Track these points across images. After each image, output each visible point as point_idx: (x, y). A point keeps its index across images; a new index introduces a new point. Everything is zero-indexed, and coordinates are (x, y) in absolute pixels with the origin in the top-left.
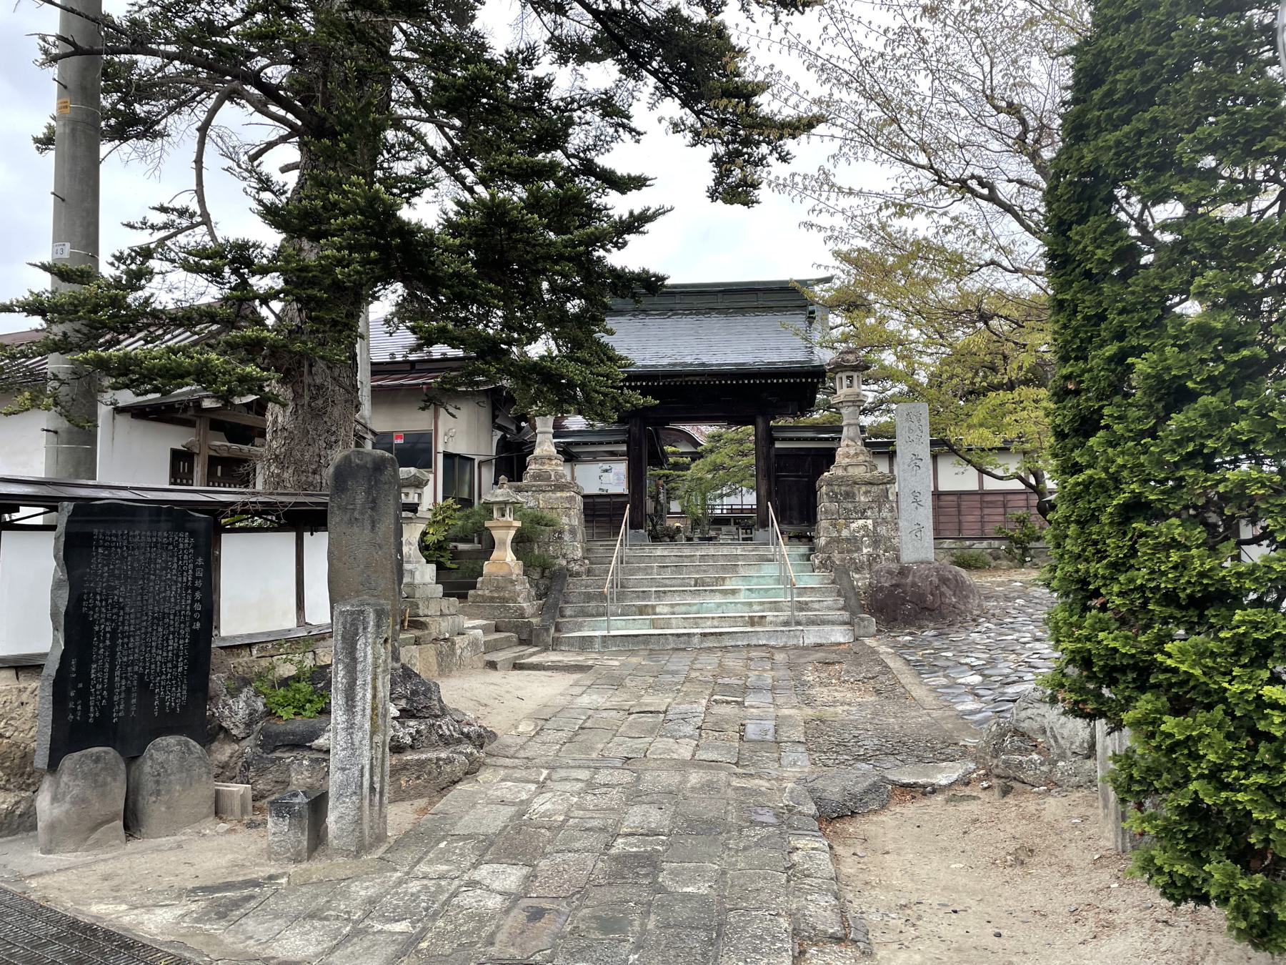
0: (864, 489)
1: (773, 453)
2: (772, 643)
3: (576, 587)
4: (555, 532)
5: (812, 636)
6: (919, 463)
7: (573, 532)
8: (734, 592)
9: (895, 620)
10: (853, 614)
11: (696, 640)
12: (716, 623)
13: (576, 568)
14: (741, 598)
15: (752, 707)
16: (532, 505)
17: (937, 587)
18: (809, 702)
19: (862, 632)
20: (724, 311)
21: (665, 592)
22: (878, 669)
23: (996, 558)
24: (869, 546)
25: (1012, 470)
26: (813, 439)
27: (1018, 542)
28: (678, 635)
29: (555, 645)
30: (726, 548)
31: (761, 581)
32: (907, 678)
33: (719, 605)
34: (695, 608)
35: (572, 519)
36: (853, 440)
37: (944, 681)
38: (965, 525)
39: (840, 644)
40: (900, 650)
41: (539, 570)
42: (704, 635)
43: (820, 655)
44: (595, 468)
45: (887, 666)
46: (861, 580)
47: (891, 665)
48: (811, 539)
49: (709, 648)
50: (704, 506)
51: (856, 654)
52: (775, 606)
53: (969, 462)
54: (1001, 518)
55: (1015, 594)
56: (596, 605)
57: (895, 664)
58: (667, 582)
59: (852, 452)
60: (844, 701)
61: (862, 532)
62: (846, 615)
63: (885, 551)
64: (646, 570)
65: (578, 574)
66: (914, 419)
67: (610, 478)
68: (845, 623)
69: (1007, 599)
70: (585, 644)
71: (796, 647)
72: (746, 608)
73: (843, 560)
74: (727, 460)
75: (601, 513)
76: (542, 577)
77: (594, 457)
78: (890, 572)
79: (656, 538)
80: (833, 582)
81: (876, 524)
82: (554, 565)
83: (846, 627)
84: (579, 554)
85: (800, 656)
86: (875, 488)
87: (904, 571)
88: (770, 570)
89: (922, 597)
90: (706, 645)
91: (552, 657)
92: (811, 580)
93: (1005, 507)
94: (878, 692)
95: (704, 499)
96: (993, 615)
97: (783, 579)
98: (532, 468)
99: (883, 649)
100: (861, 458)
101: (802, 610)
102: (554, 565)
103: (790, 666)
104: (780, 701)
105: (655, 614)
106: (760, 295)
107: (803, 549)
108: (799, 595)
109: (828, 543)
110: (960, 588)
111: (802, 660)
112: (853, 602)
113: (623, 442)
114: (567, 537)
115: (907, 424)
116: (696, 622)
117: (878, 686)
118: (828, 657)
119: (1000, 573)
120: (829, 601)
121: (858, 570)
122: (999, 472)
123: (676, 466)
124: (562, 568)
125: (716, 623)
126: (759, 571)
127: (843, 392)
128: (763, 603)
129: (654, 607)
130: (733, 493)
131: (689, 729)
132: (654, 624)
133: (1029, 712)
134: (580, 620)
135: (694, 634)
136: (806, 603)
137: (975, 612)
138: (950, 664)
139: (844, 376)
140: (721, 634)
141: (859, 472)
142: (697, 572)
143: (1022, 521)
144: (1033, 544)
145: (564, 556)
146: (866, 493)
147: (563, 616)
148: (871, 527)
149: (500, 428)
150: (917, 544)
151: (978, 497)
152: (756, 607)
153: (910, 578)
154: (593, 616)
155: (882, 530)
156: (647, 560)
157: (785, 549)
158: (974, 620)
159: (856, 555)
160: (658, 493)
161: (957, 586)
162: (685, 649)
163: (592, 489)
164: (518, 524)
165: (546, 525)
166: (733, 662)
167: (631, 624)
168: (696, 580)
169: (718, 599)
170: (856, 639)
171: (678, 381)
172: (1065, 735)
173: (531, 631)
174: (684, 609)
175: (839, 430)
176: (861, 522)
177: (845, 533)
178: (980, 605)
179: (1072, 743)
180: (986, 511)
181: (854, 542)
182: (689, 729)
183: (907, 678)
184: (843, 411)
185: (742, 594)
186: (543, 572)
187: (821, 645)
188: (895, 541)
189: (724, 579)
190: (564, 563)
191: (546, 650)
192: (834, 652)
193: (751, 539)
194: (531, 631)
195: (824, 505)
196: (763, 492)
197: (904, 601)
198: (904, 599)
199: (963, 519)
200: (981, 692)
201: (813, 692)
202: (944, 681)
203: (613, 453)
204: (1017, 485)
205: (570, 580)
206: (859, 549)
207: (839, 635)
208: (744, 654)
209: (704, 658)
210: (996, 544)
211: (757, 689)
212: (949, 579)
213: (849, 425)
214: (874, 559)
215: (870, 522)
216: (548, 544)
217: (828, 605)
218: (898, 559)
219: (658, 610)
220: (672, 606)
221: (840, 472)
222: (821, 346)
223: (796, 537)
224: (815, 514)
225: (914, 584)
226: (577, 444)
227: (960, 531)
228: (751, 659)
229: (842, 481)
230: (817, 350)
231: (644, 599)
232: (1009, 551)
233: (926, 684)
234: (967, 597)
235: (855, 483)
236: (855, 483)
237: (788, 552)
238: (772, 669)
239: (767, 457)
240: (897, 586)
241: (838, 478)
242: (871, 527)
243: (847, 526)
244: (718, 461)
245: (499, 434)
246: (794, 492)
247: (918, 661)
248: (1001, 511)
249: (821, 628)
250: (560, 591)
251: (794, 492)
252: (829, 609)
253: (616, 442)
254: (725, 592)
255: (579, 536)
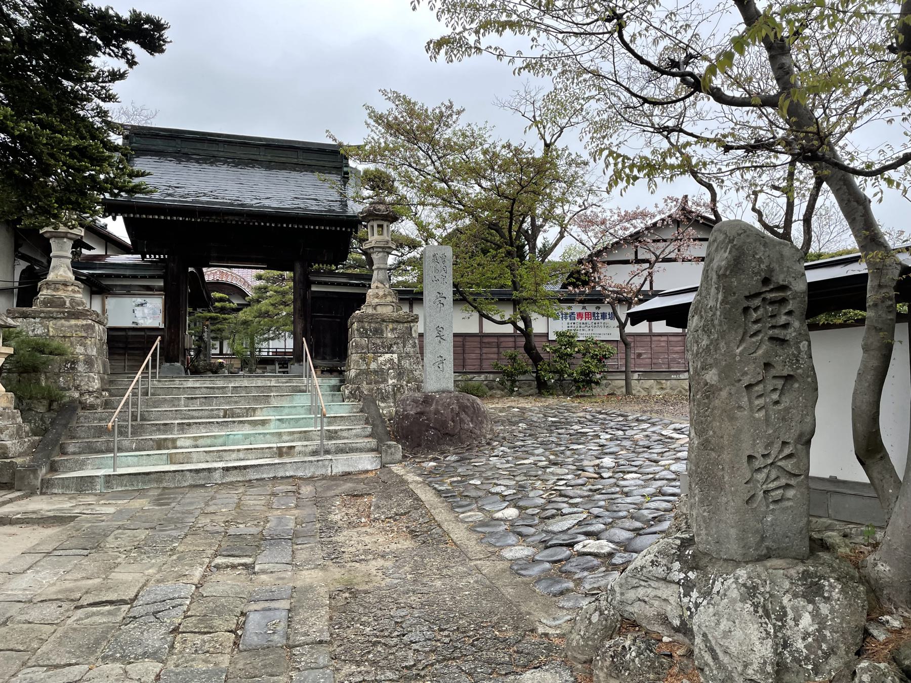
0: (391, 326)
1: (308, 295)
2: (300, 474)
3: (86, 421)
4: (67, 361)
5: (341, 464)
6: (443, 300)
7: (89, 362)
8: (263, 423)
9: (419, 445)
10: (380, 441)
11: (217, 475)
12: (241, 455)
13: (90, 400)
14: (271, 429)
15: (263, 572)
16: (39, 332)
17: (458, 415)
18: (335, 556)
19: (389, 458)
20: (269, 166)
21: (189, 424)
22: (409, 502)
23: (491, 388)
24: (394, 378)
25: (506, 318)
26: (345, 284)
27: (510, 375)
28: (197, 471)
29: (45, 488)
30: (271, 381)
31: (293, 411)
32: (441, 514)
33: (247, 437)
34: (220, 441)
35: (90, 348)
36: (382, 283)
37: (480, 516)
38: (468, 362)
39: (367, 471)
40: (428, 477)
41: (45, 402)
42: (227, 469)
43: (348, 486)
44: (129, 302)
45: (418, 499)
46: (387, 409)
47: (423, 497)
48: (341, 373)
49: (232, 483)
50: (253, 349)
51: (386, 485)
52: (305, 436)
53: (475, 308)
54: (495, 356)
55: (517, 419)
56: (102, 443)
57: (426, 495)
58: (195, 414)
59: (381, 293)
60: (375, 551)
61: (388, 365)
62: (373, 443)
63: (408, 382)
64: (173, 402)
65: (92, 407)
66: (440, 260)
67: (146, 312)
68: (372, 450)
69: (512, 423)
70: (84, 485)
71: (324, 477)
72: (275, 439)
73: (371, 390)
74: (271, 308)
75: (125, 345)
76: (50, 409)
77: (128, 291)
78: (415, 401)
79: (195, 371)
80: (361, 411)
81: (400, 358)
82: (62, 397)
83: (373, 454)
84: (96, 385)
85: (329, 488)
86: (400, 326)
87: (428, 400)
88: (302, 400)
89: (444, 424)
90: (228, 479)
91: (39, 505)
92: (342, 409)
93: (498, 347)
94: (413, 534)
95: (252, 343)
96: (504, 438)
97: (313, 409)
98: (45, 293)
99: (411, 477)
100: (389, 299)
101: (330, 438)
102: (62, 397)
103: (318, 501)
104: (302, 556)
105: (176, 448)
106: (300, 153)
107: (334, 381)
108: (329, 424)
109: (356, 376)
110: (477, 415)
111: (332, 493)
112: (380, 429)
113: (159, 277)
114: (81, 367)
115: (433, 265)
116: (220, 455)
117: (413, 526)
118: (355, 487)
119: (496, 400)
120: (358, 428)
121: (383, 399)
122: (497, 318)
123: (223, 310)
124: (73, 401)
125: (241, 455)
126: (291, 401)
127: (374, 238)
128: (293, 433)
129: (174, 441)
130: (276, 337)
131: (155, 637)
132: (171, 459)
133: (641, 592)
134: (82, 457)
135: (215, 469)
136: (336, 432)
137: (489, 436)
138: (480, 494)
139: (375, 224)
140: (245, 467)
141: (387, 311)
142: (229, 403)
143: (513, 358)
144: (521, 377)
145: (77, 388)
146: (393, 330)
147: (64, 453)
148: (396, 361)
149: (24, 257)
150: (439, 376)
151: (478, 339)
152: (285, 438)
153: (433, 407)
154: (102, 452)
155: (406, 364)
156: (175, 391)
157: (317, 381)
158: (488, 444)
159: (382, 386)
160: (203, 332)
161: (474, 412)
162: (203, 486)
163: (125, 322)
164: (10, 351)
165: (51, 353)
166: (254, 500)
167: (144, 460)
168: (225, 411)
169: (247, 430)
170: (383, 466)
171: (214, 219)
172: (733, 650)
173: (14, 474)
174: (209, 441)
175: (369, 278)
176: (388, 356)
177: (373, 366)
178: (492, 430)
179: (746, 666)
180: (485, 350)
181: (380, 373)
182: (155, 637)
183: (441, 514)
184: (374, 256)
185: (272, 425)
186: (50, 405)
187: (349, 473)
188: (417, 373)
189: (254, 410)
190: (77, 395)
191: (32, 493)
192: (363, 481)
193: (287, 372)
194: (14, 474)
195: (355, 339)
196: (299, 330)
197: (428, 427)
198: (428, 425)
199: (466, 356)
200: (525, 530)
201: (340, 538)
202: (480, 516)
203: (149, 288)
204: (509, 329)
205: (80, 413)
206: (385, 381)
207: (366, 462)
208: (269, 489)
209: (224, 493)
210: (491, 377)
211: (275, 540)
212: (467, 407)
213: (379, 269)
214: (399, 389)
215: (395, 356)
216: (58, 375)
217: (357, 433)
218: (418, 389)
219: (179, 443)
220: (195, 438)
221: (370, 311)
222: (355, 201)
223: (327, 371)
224: (346, 349)
225: (437, 412)
226: (108, 276)
227: (464, 367)
228: (274, 494)
229: (372, 318)
230: (350, 203)
231: (165, 432)
232: (502, 383)
233: (463, 521)
234: (482, 422)
235: (384, 321)
236: (384, 321)
237: (320, 383)
238: (297, 506)
239: (304, 300)
240: (421, 414)
241: (368, 315)
242: (396, 361)
243: (375, 359)
244: (263, 309)
245: (22, 265)
246: (326, 330)
247: (448, 491)
248: (495, 350)
249: (350, 456)
250: (65, 426)
251: (326, 330)
252: (357, 436)
253: (152, 277)
254: (254, 423)
255: (98, 366)
